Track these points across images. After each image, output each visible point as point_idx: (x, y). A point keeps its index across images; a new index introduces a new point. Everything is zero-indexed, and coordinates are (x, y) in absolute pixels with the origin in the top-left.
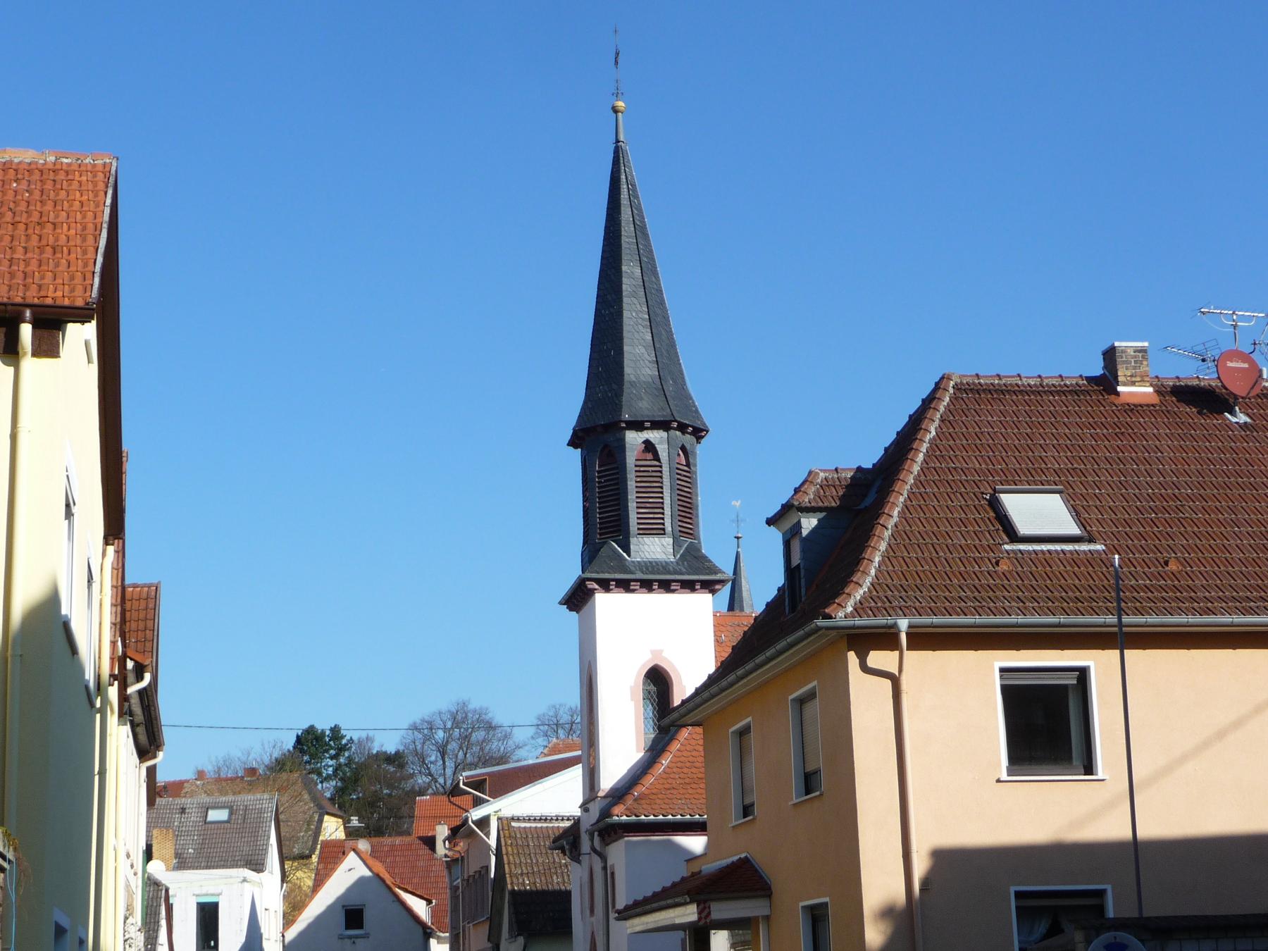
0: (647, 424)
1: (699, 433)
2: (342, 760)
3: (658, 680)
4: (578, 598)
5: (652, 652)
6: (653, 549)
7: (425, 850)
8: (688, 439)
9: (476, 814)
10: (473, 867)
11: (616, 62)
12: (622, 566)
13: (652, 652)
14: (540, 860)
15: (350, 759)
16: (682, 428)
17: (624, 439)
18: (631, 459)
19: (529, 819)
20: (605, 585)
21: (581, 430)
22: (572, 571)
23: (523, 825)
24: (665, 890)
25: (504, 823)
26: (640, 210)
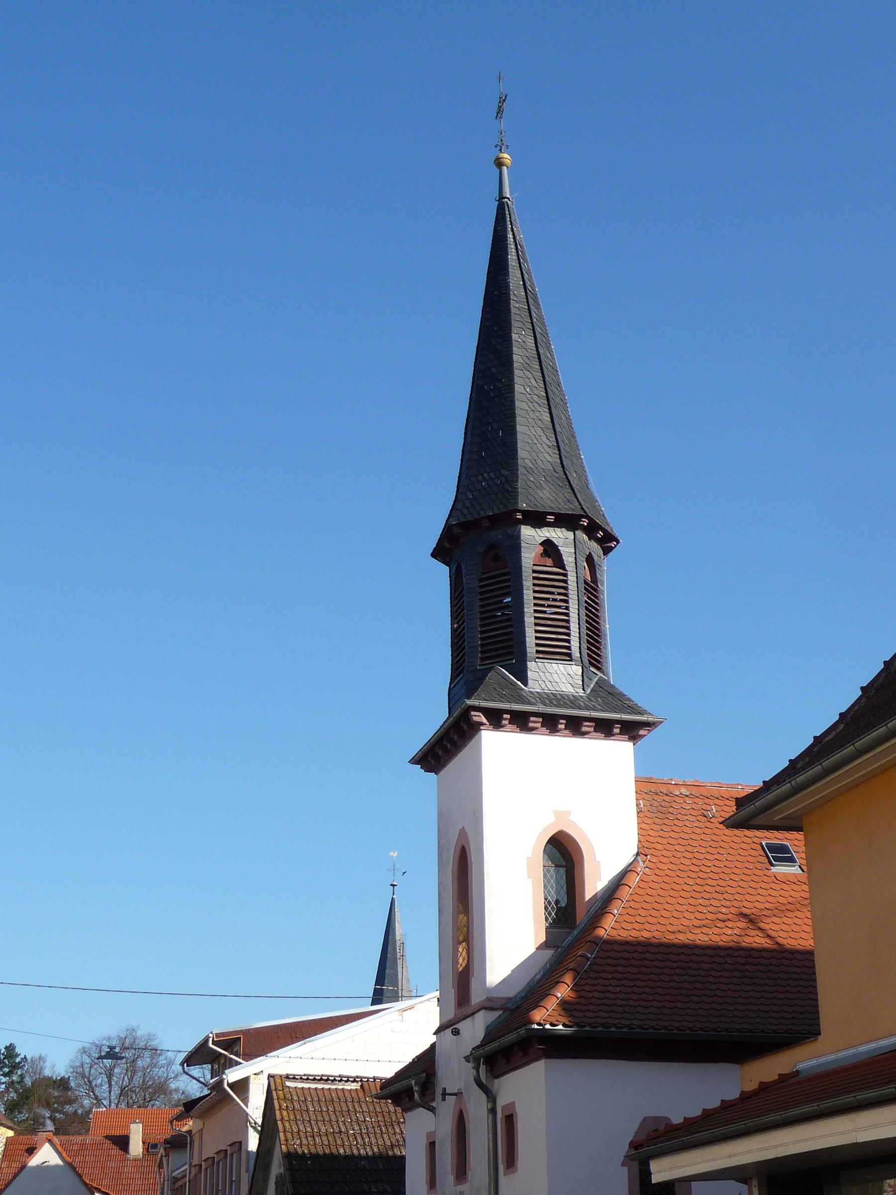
0: (551, 518)
1: (607, 541)
2: (15, 1078)
3: (563, 853)
4: (444, 749)
5: (557, 814)
6: (555, 678)
7: (116, 1151)
8: (595, 548)
9: (232, 1075)
10: (211, 1144)
11: (500, 111)
12: (520, 698)
13: (557, 814)
14: (323, 1129)
15: (22, 1077)
16: (592, 529)
17: (518, 537)
18: (529, 557)
19: (307, 1079)
20: (495, 719)
21: (460, 525)
22: (435, 716)
23: (300, 1085)
24: (707, 1114)
25: (275, 1084)
26: (529, 273)
